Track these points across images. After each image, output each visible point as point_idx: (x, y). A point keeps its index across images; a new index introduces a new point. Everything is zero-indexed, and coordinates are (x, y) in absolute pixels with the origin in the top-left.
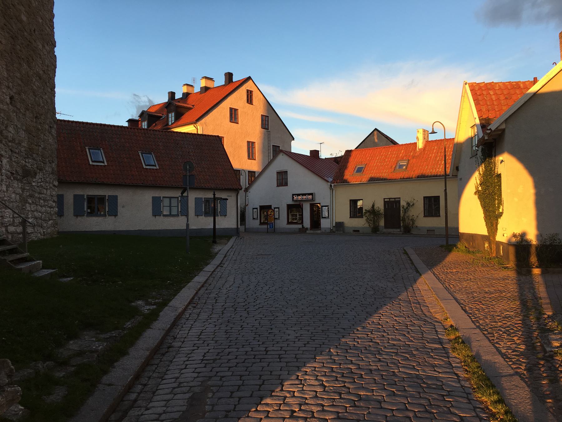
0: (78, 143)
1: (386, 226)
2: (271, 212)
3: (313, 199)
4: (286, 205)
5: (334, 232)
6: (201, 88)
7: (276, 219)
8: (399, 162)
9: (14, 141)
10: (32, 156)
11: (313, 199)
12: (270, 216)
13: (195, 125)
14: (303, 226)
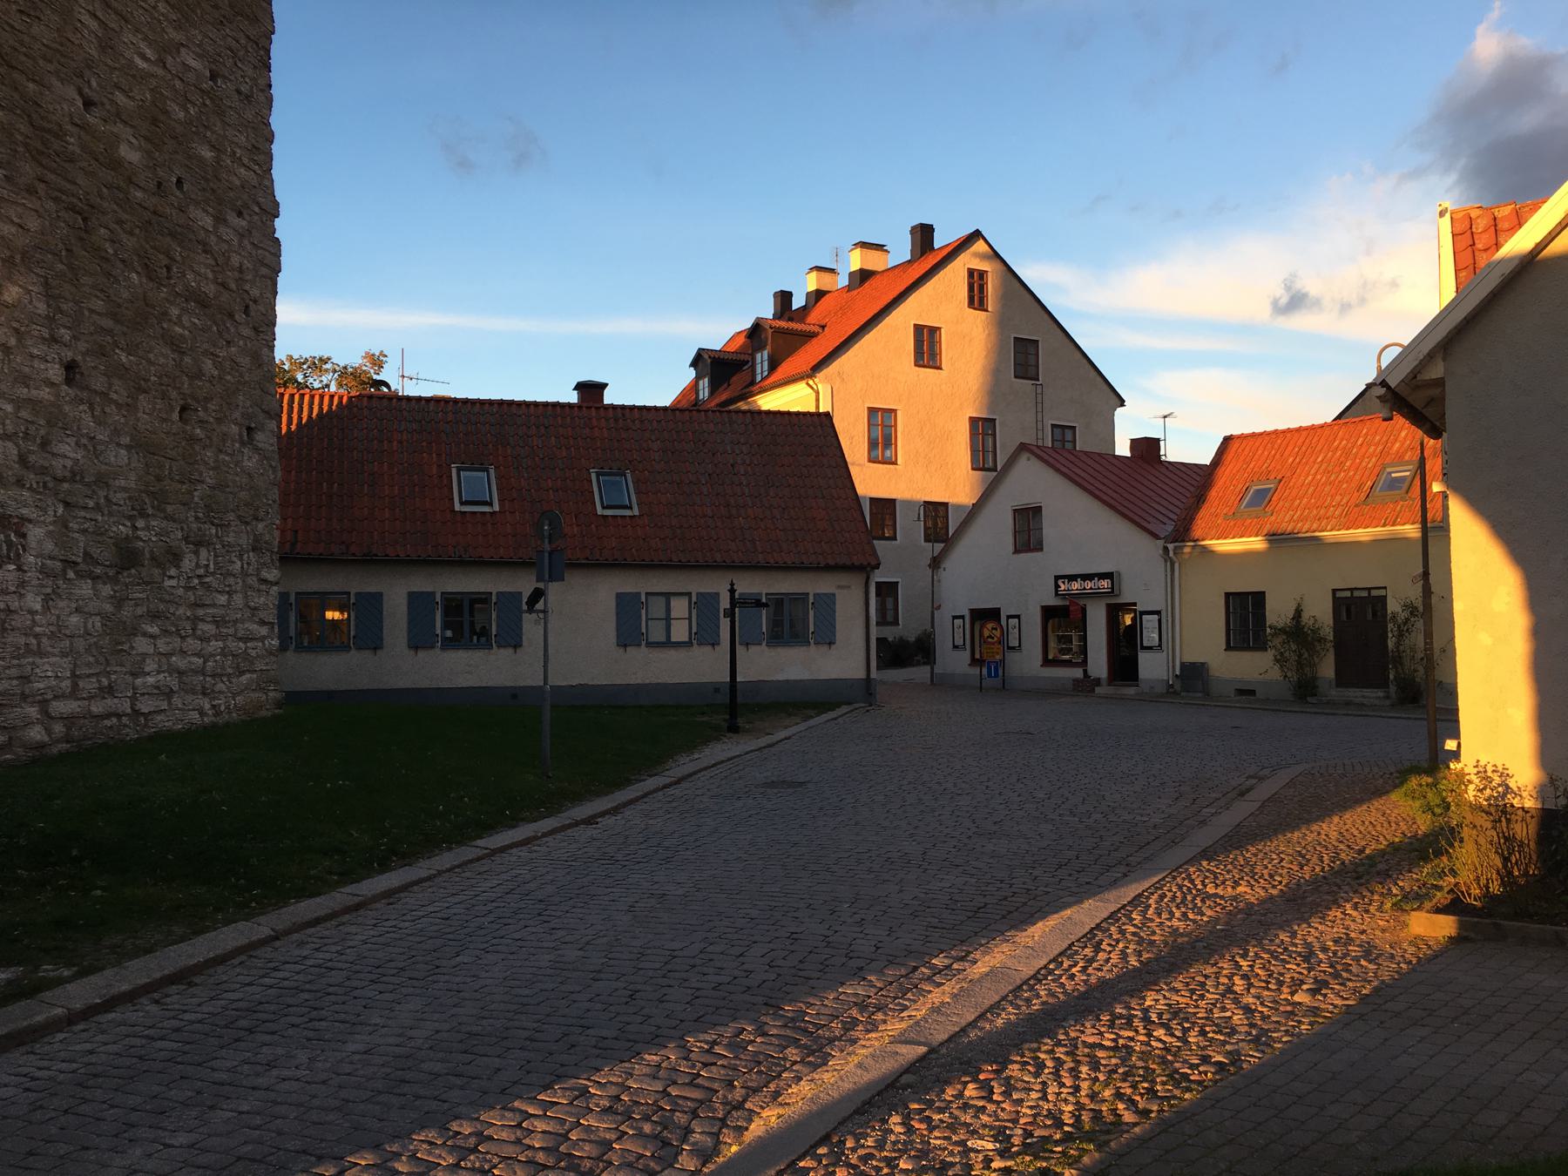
0: (434, 455)
1: (1342, 680)
2: (993, 629)
3: (1112, 592)
4: (1039, 609)
5: (1175, 693)
6: (851, 274)
7: (1013, 648)
8: (1389, 470)
9: (78, 478)
10: (164, 511)
11: (1113, 592)
12: (990, 640)
13: (811, 382)
14: (1085, 672)
